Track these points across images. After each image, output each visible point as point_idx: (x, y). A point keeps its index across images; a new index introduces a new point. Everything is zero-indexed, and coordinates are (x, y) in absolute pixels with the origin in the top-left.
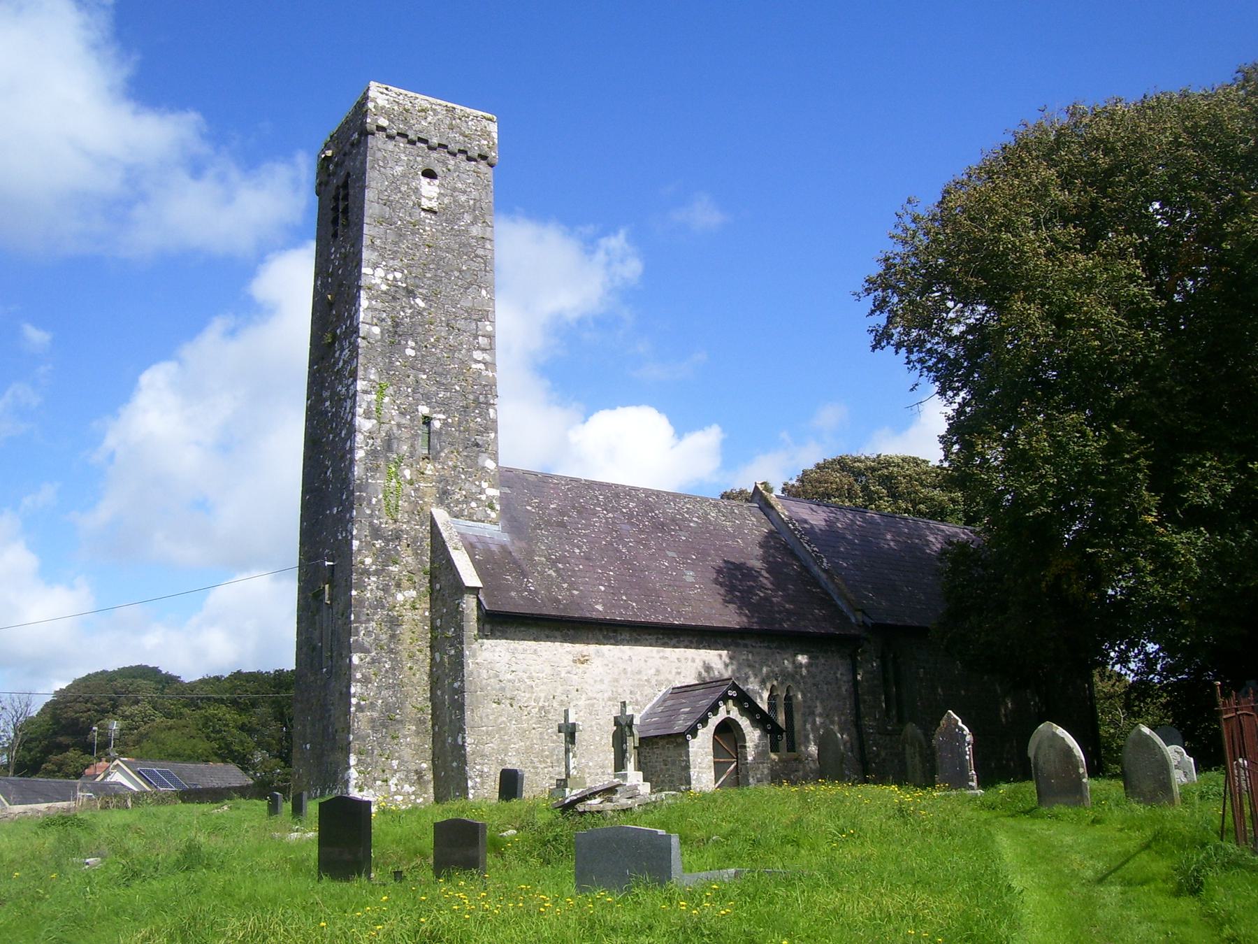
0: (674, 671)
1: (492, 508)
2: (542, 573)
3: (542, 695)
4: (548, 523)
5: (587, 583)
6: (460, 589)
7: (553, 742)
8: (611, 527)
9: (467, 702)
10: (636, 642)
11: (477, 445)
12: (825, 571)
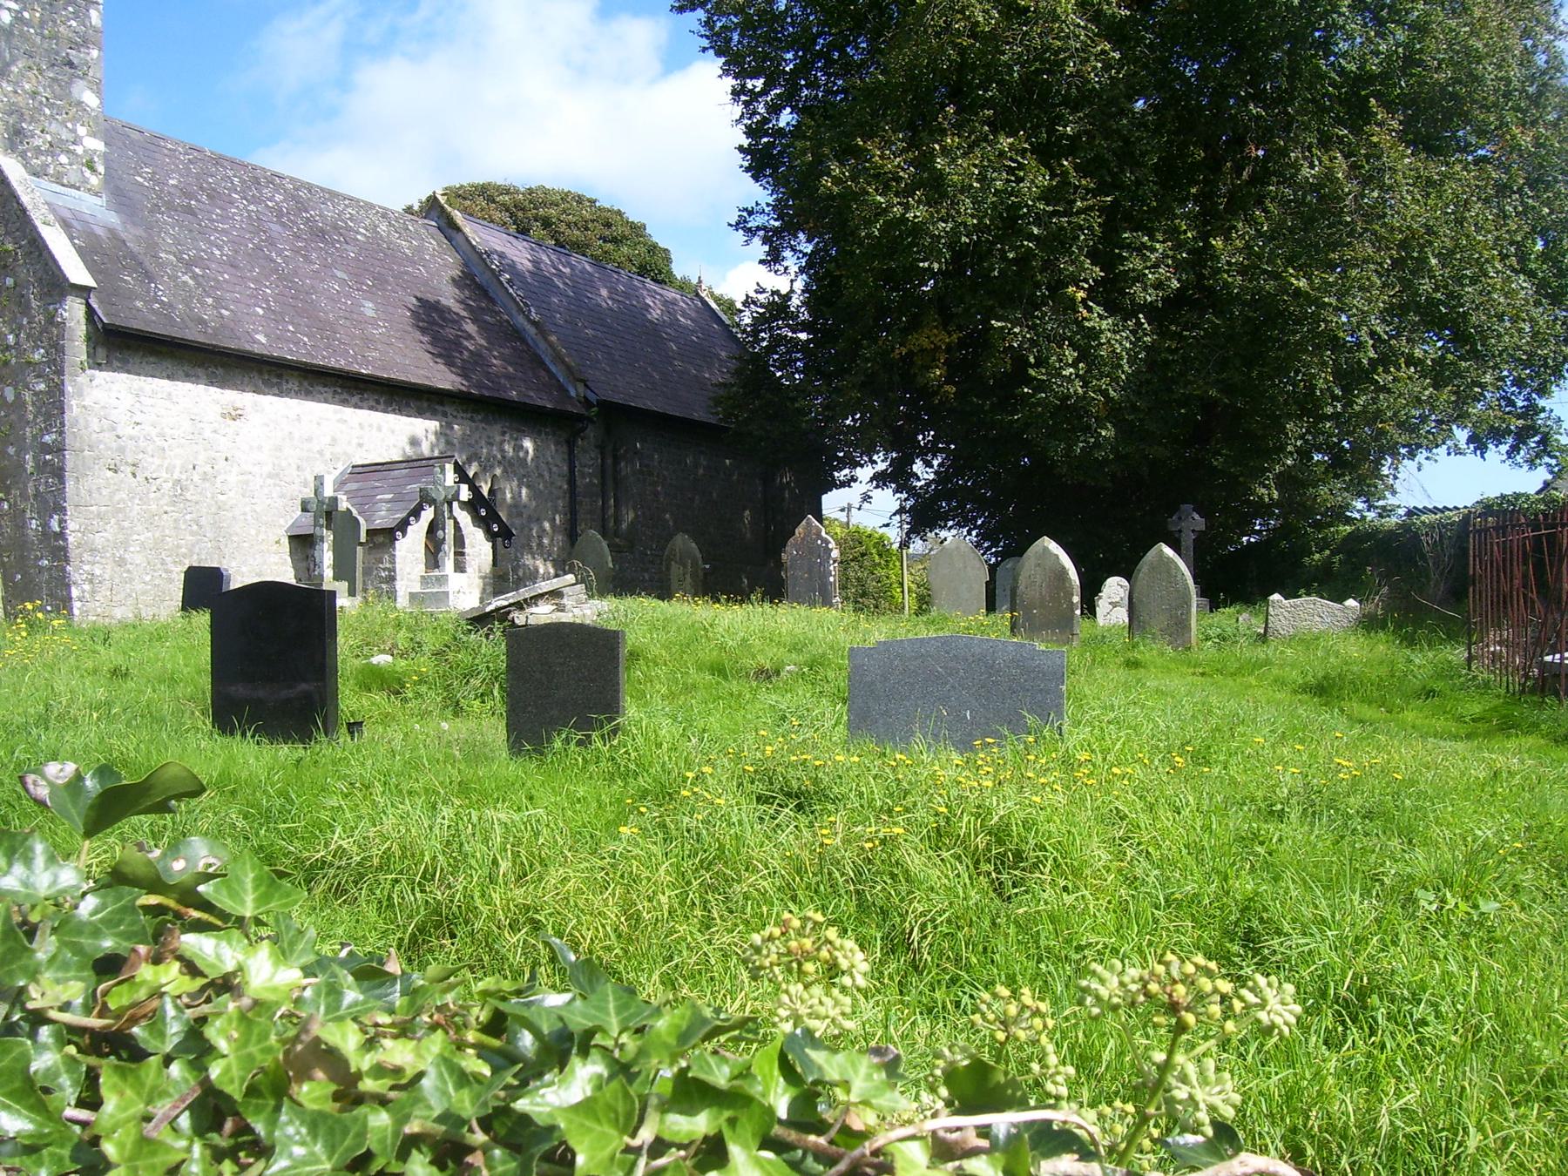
0: (355, 441)
1: (93, 170)
2: (174, 278)
3: (178, 463)
4: (170, 207)
5: (236, 301)
6: (57, 286)
7: (192, 534)
8: (256, 224)
9: (69, 465)
10: (307, 394)
11: (71, 64)
12: (534, 323)
